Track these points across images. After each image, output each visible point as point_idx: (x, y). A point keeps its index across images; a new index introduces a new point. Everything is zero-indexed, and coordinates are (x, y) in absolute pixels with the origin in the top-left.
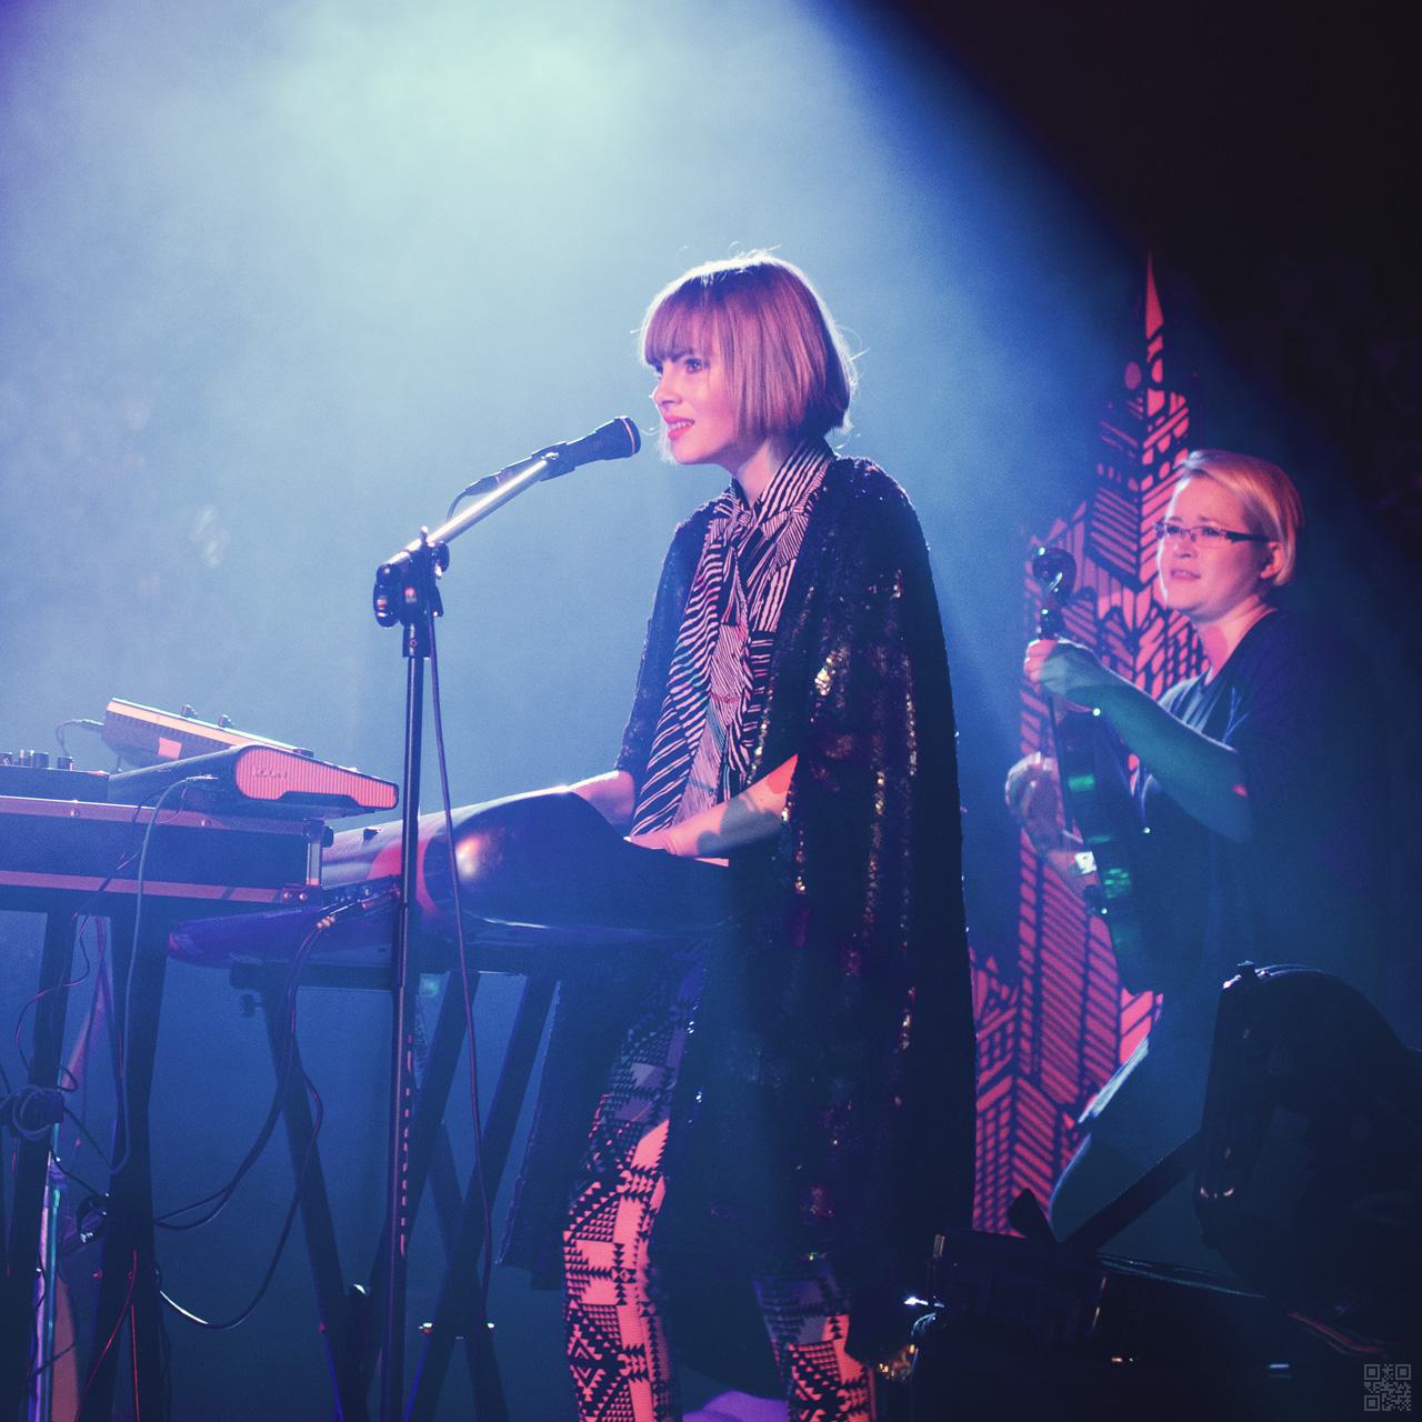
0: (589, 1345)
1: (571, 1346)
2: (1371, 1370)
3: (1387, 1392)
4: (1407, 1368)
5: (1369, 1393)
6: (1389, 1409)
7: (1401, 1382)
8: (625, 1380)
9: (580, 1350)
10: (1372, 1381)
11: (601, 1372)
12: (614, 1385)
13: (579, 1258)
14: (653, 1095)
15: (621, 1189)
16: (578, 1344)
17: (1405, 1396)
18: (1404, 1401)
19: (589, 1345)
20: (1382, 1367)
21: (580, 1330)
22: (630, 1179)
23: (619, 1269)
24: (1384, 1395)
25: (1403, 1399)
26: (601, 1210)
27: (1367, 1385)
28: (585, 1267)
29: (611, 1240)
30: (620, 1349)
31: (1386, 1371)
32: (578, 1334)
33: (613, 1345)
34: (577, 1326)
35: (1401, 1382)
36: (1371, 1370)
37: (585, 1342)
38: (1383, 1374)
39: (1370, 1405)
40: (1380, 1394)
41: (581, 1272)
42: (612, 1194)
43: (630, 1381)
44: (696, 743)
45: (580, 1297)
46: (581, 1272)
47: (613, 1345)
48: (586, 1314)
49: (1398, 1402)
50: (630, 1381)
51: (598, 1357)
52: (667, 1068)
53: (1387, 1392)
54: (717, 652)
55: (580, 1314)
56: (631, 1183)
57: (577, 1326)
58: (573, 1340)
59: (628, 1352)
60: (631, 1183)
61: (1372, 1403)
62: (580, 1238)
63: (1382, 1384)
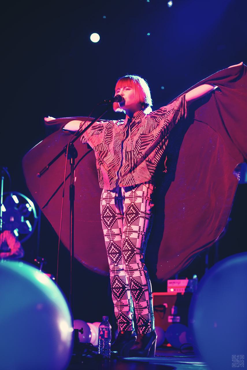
0: (135, 286)
1: (132, 287)
2: (234, 357)
3: (238, 362)
4: (243, 356)
5: (233, 363)
6: (238, 367)
7: (241, 360)
8: (139, 217)
9: (134, 287)
10: (234, 359)
11: (138, 291)
12: (147, 330)
13: (131, 268)
14: (147, 307)
15: (143, 290)
16: (133, 286)
17: (243, 363)
18: (243, 364)
19: (135, 286)
20: (237, 356)
21: (133, 283)
22: (144, 288)
23: (139, 268)
24: (237, 363)
25: (242, 364)
26: (142, 295)
27: (233, 360)
28: (142, 307)
29: (136, 263)
30: (142, 285)
31: (238, 357)
32: (133, 284)
33: (141, 285)
34: (132, 282)
35: (241, 360)
36: (234, 357)
37: (135, 285)
38: (237, 357)
39: (234, 365)
40: (236, 363)
41: (132, 270)
42: (142, 292)
43: (140, 217)
44: (133, 178)
45: (141, 314)
46: (132, 270)
47: (141, 285)
48: (134, 279)
49: (241, 365)
50: (140, 217)
51: (138, 288)
52: (139, 226)
53: (238, 362)
54: (135, 179)
55: (133, 279)
56: (144, 288)
57: (132, 282)
58: (132, 285)
59: (144, 286)
60: (144, 288)
61: (234, 365)
62: (140, 302)
63: (237, 360)
